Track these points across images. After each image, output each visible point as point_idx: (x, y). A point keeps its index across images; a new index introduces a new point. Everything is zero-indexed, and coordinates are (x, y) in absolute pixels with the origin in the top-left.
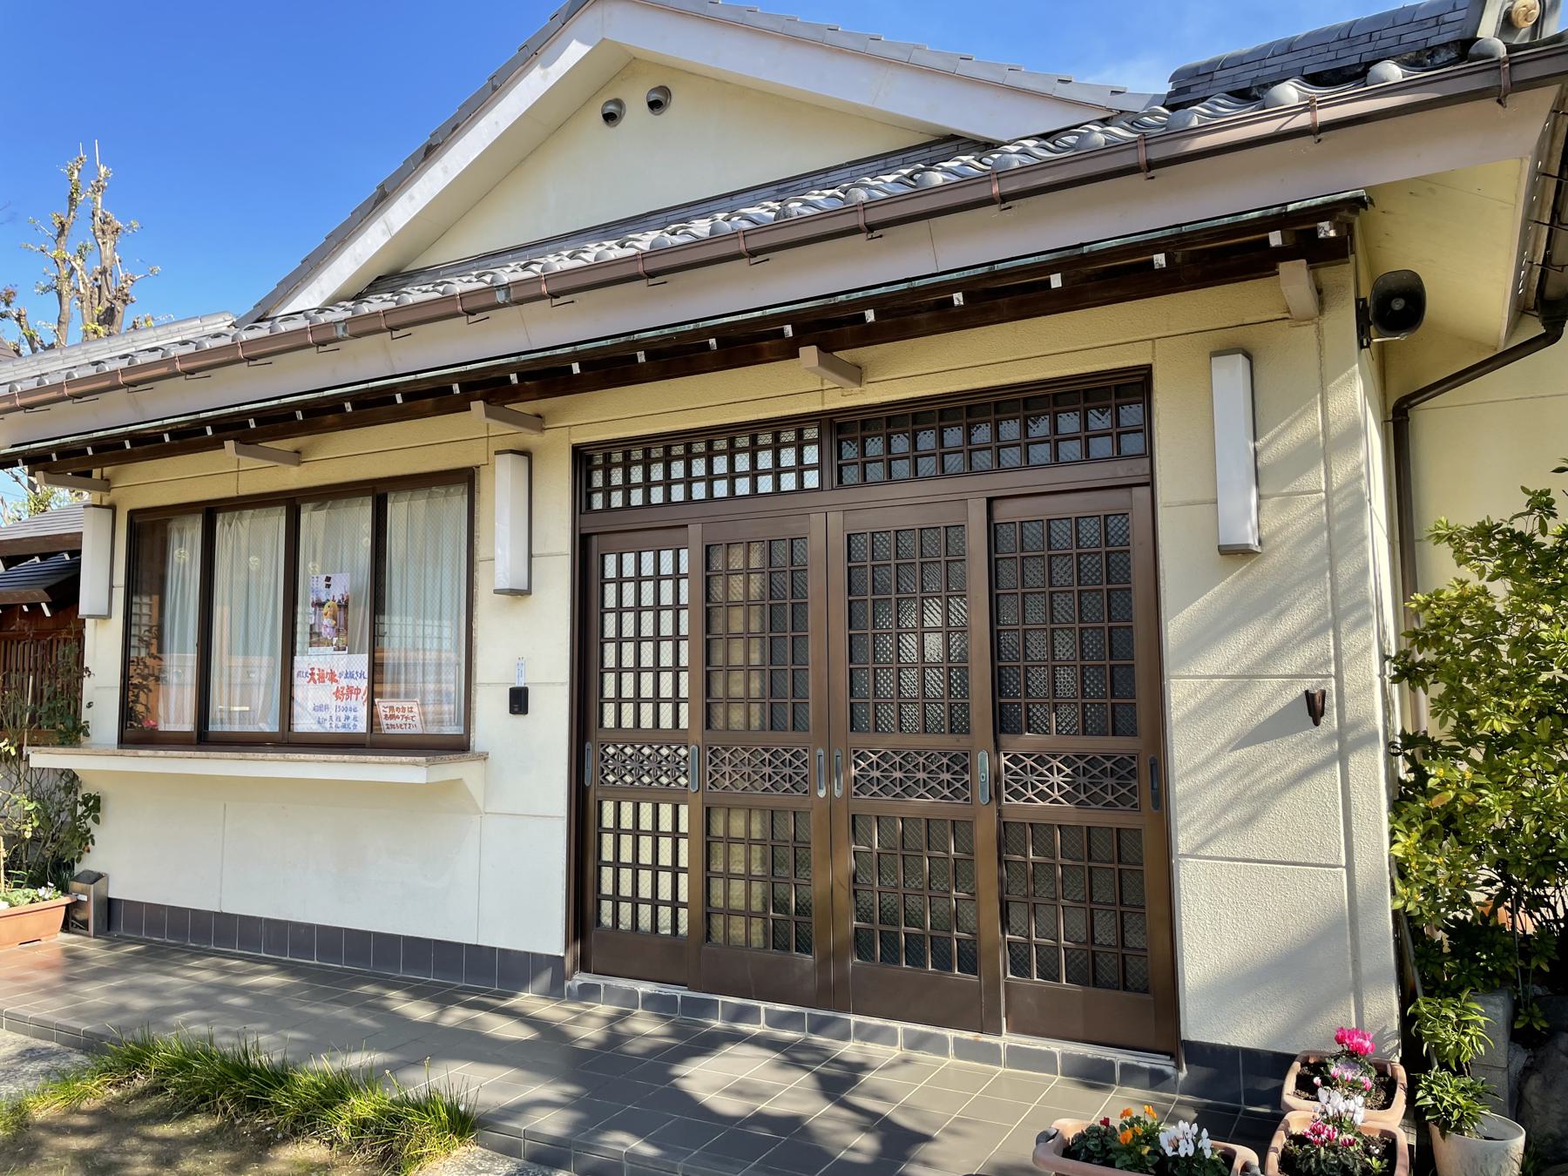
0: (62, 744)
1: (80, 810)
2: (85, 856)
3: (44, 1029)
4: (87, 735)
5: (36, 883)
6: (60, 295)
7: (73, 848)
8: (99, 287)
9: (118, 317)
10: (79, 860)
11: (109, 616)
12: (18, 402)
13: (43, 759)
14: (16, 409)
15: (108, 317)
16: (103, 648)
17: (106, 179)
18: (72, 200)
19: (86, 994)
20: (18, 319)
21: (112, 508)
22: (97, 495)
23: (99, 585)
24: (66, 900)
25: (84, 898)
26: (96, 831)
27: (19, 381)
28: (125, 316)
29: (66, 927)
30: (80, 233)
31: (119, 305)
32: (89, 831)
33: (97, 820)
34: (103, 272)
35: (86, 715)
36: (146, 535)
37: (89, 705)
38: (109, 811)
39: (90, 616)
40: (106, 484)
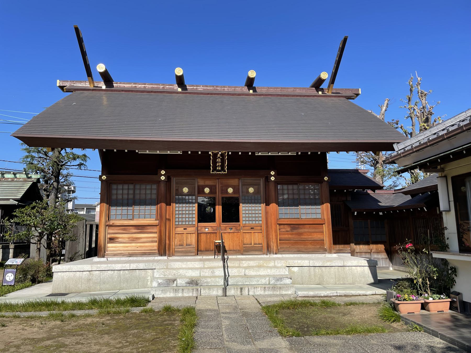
0: (441, 251)
1: (450, 272)
2: (453, 286)
3: (452, 341)
4: (449, 248)
5: (440, 293)
6: (411, 118)
7: (449, 283)
8: (423, 113)
9: (430, 120)
10: (452, 287)
11: (450, 211)
12: (414, 150)
13: (436, 255)
14: (414, 152)
15: (427, 120)
16: (450, 221)
17: (420, 80)
18: (411, 90)
19: (464, 332)
20: (401, 128)
21: (446, 177)
22: (440, 173)
23: (445, 201)
24: (450, 300)
25: (456, 300)
26: (456, 278)
27: (413, 144)
28: (432, 118)
29: (450, 309)
30: (415, 98)
31: (429, 116)
32: (453, 278)
33: (456, 275)
34: (424, 108)
35: (447, 242)
36: (458, 183)
37: (448, 239)
38: (461, 272)
39: (444, 211)
40: (442, 170)
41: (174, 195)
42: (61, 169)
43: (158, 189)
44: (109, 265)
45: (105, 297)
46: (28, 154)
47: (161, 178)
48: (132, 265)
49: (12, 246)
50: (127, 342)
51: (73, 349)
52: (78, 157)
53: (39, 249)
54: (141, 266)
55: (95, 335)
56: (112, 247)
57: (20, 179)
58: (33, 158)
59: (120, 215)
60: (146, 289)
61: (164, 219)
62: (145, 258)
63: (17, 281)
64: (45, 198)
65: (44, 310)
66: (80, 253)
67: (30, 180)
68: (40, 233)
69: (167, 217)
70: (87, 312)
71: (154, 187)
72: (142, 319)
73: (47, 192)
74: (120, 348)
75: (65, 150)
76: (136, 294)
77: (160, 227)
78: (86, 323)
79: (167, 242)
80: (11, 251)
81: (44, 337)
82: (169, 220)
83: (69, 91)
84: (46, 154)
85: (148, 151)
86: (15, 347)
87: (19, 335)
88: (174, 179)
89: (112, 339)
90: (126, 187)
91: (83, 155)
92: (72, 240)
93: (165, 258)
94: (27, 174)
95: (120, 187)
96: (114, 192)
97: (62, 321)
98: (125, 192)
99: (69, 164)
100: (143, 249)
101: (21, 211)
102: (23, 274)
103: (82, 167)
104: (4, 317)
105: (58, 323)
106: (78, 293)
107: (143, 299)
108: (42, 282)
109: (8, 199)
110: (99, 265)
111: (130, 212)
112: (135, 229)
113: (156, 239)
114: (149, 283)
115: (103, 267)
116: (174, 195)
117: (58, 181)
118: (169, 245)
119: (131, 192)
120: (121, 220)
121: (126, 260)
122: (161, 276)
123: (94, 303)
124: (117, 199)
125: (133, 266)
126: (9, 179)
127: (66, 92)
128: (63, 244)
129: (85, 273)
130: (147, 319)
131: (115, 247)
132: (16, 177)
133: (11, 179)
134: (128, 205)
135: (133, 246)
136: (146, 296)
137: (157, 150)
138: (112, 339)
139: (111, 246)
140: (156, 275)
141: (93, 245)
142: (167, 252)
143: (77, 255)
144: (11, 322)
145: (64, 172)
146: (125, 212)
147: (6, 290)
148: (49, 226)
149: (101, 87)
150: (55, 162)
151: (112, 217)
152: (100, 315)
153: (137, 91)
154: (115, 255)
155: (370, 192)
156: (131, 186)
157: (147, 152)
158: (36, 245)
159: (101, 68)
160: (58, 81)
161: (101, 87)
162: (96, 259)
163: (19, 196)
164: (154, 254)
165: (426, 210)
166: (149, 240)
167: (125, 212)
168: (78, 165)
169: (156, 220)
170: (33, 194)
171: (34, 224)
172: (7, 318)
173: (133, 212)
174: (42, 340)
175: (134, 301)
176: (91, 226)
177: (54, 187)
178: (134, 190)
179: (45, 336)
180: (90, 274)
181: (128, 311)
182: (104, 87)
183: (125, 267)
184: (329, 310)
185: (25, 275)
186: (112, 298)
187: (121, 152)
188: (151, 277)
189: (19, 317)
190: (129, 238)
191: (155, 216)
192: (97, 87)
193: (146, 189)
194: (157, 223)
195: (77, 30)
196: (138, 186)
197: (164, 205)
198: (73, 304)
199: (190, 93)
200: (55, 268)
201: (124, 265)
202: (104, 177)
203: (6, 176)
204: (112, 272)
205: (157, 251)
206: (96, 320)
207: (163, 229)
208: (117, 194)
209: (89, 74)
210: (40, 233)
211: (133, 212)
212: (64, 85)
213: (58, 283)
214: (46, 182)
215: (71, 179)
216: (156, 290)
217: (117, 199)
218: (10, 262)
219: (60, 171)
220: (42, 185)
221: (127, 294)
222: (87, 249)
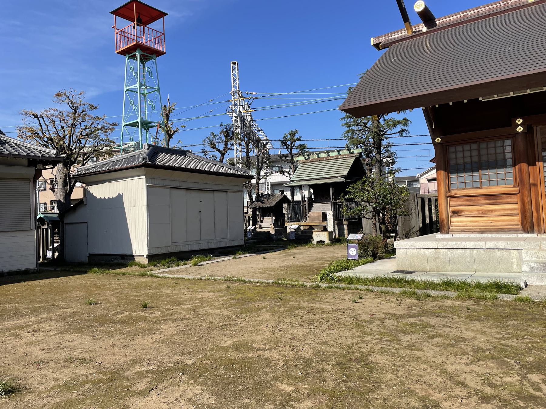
41: (540, 150)
42: (382, 139)
43: (513, 146)
44: (458, 243)
45: (461, 279)
46: (348, 129)
47: (517, 129)
48: (488, 243)
49: (345, 222)
50: (508, 333)
51: (442, 331)
52: (399, 123)
53: (375, 224)
54: (502, 245)
55: (462, 319)
56: (457, 222)
58: (353, 131)
59: (463, 184)
60: (511, 274)
61: (527, 185)
62: (503, 236)
63: (360, 256)
64: (368, 172)
65: (395, 287)
66: (415, 229)
67: (353, 155)
68: (374, 208)
69: (532, 181)
70: (443, 293)
71: (508, 142)
72: (519, 309)
73: (370, 166)
74: (499, 339)
75: (384, 117)
76: (501, 279)
77: (522, 195)
78: (446, 305)
79: (535, 214)
80: (346, 227)
81: (404, 314)
82: (535, 185)
83: (385, 46)
84: (365, 125)
85: (496, 96)
86: (379, 320)
87: (378, 308)
88: (538, 128)
89: (485, 327)
90: (467, 147)
91: (404, 119)
92: (405, 215)
93: (534, 235)
94: (349, 150)
95: (459, 148)
96: (453, 156)
97: (418, 300)
98: (467, 154)
99: (389, 132)
100: (500, 223)
101: (353, 187)
102: (364, 250)
103: (404, 134)
104: (358, 289)
105: (415, 301)
106: (425, 272)
107: (512, 286)
108: (383, 259)
109: (336, 177)
110: (445, 243)
111: (476, 179)
112: (485, 199)
113: (518, 212)
114: (515, 266)
115: (451, 244)
116: (540, 150)
117: (379, 153)
118: (539, 219)
119: (475, 153)
120: (465, 189)
121: (476, 238)
122: (534, 259)
123: (448, 284)
124: (457, 164)
125: (490, 245)
126: (333, 157)
127: (382, 49)
128: (394, 218)
129: (430, 250)
130: (527, 310)
131: (461, 222)
132: (340, 154)
133: (336, 156)
134: (473, 170)
135: (484, 221)
136: (516, 282)
137: (509, 92)
138: (485, 327)
139: (455, 221)
140: (525, 256)
141: (428, 221)
142: (536, 228)
143: (412, 231)
144: (366, 295)
145: (384, 142)
146: (469, 179)
147: (353, 264)
148: (383, 200)
149: (421, 30)
150: (376, 132)
151: (452, 187)
152: (460, 297)
153: (469, 21)
154: (462, 231)
156: (474, 146)
157: (496, 97)
158: (371, 221)
159: (419, 6)
160: (372, 39)
161: (421, 30)
162: (438, 235)
163: (346, 173)
164: (516, 231)
165: (331, 188)
166: (508, 212)
167: (469, 179)
168: (399, 132)
169: (514, 186)
170: (357, 171)
171: (367, 199)
172: (361, 290)
173: (481, 178)
174: (404, 316)
175: (499, 287)
176: (423, 200)
177: (377, 160)
178: (479, 150)
179: (405, 313)
180: (437, 252)
181: (495, 298)
182: (425, 29)
183: (479, 245)
184: (531, 359)
185: (366, 250)
186: (469, 280)
187: (459, 104)
188: (516, 259)
189: (372, 291)
190: (478, 211)
191: (512, 182)
192: (416, 32)
193: (495, 147)
194: (516, 191)
196: (483, 145)
197: (524, 166)
199: (441, 29)
200: (397, 244)
201: (477, 243)
202: (438, 140)
203: (331, 154)
204: (463, 251)
205: (520, 227)
206: (457, 303)
207: (526, 197)
208: (456, 158)
209: (406, 19)
210: (374, 208)
211: (481, 178)
212: (379, 42)
213: (401, 260)
214: (368, 156)
215: (392, 149)
216: (528, 276)
217: (457, 164)
218: (351, 237)
219: (381, 141)
220: (364, 160)
221: (489, 277)
222: (421, 225)
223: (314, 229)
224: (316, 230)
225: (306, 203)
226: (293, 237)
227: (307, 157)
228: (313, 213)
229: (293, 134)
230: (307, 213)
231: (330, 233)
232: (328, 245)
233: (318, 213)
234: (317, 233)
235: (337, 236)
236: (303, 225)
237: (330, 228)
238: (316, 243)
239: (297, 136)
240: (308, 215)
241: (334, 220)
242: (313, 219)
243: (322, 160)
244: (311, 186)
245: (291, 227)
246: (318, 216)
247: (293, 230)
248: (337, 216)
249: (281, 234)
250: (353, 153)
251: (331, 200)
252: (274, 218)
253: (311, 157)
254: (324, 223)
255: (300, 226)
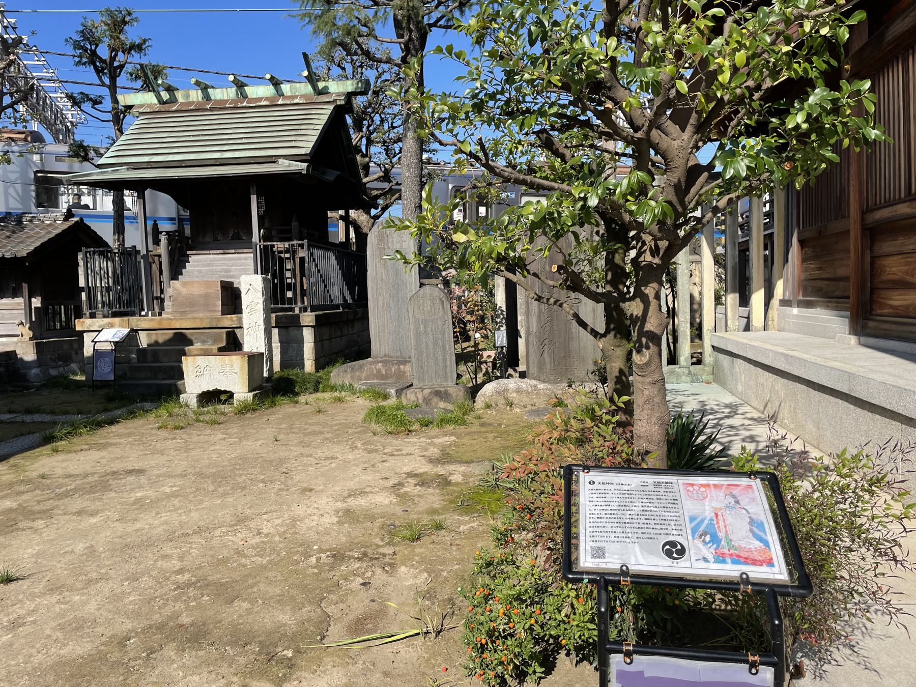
49: (308, 318)
57: (295, 97)
94: (312, 79)
109: (272, 160)
126: (260, 99)
132: (280, 94)
133: (267, 99)
155: (652, 152)
163: (307, 145)
165: (254, 198)
195: (305, 56)
198: (761, 565)
223: (191, 343)
224: (197, 346)
225: (163, 249)
226: (105, 371)
227: (165, 96)
228: (185, 284)
229: (118, 24)
230: (165, 285)
231: (254, 360)
232: (245, 409)
233: (207, 284)
234: (201, 361)
235: (277, 367)
236: (149, 329)
237: (254, 338)
238: (193, 402)
239: (131, 35)
240: (169, 292)
241: (268, 311)
242: (188, 305)
243: (220, 107)
244: (457, 365)
245: (102, 334)
246: (206, 296)
247: (109, 347)
248: (276, 294)
249: (66, 359)
250: (324, 92)
251: (255, 238)
252: (36, 302)
253: (180, 96)
254: (229, 321)
255: (134, 332)
